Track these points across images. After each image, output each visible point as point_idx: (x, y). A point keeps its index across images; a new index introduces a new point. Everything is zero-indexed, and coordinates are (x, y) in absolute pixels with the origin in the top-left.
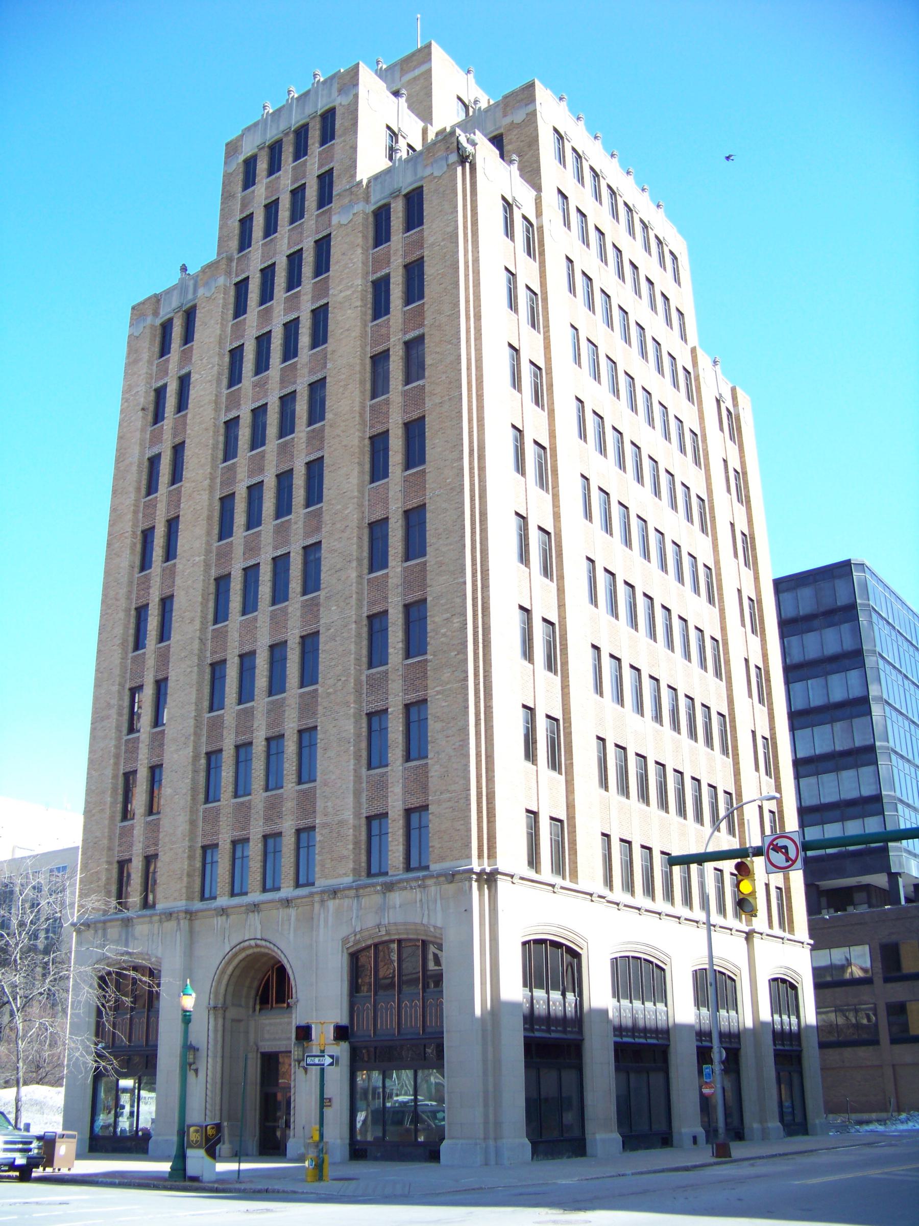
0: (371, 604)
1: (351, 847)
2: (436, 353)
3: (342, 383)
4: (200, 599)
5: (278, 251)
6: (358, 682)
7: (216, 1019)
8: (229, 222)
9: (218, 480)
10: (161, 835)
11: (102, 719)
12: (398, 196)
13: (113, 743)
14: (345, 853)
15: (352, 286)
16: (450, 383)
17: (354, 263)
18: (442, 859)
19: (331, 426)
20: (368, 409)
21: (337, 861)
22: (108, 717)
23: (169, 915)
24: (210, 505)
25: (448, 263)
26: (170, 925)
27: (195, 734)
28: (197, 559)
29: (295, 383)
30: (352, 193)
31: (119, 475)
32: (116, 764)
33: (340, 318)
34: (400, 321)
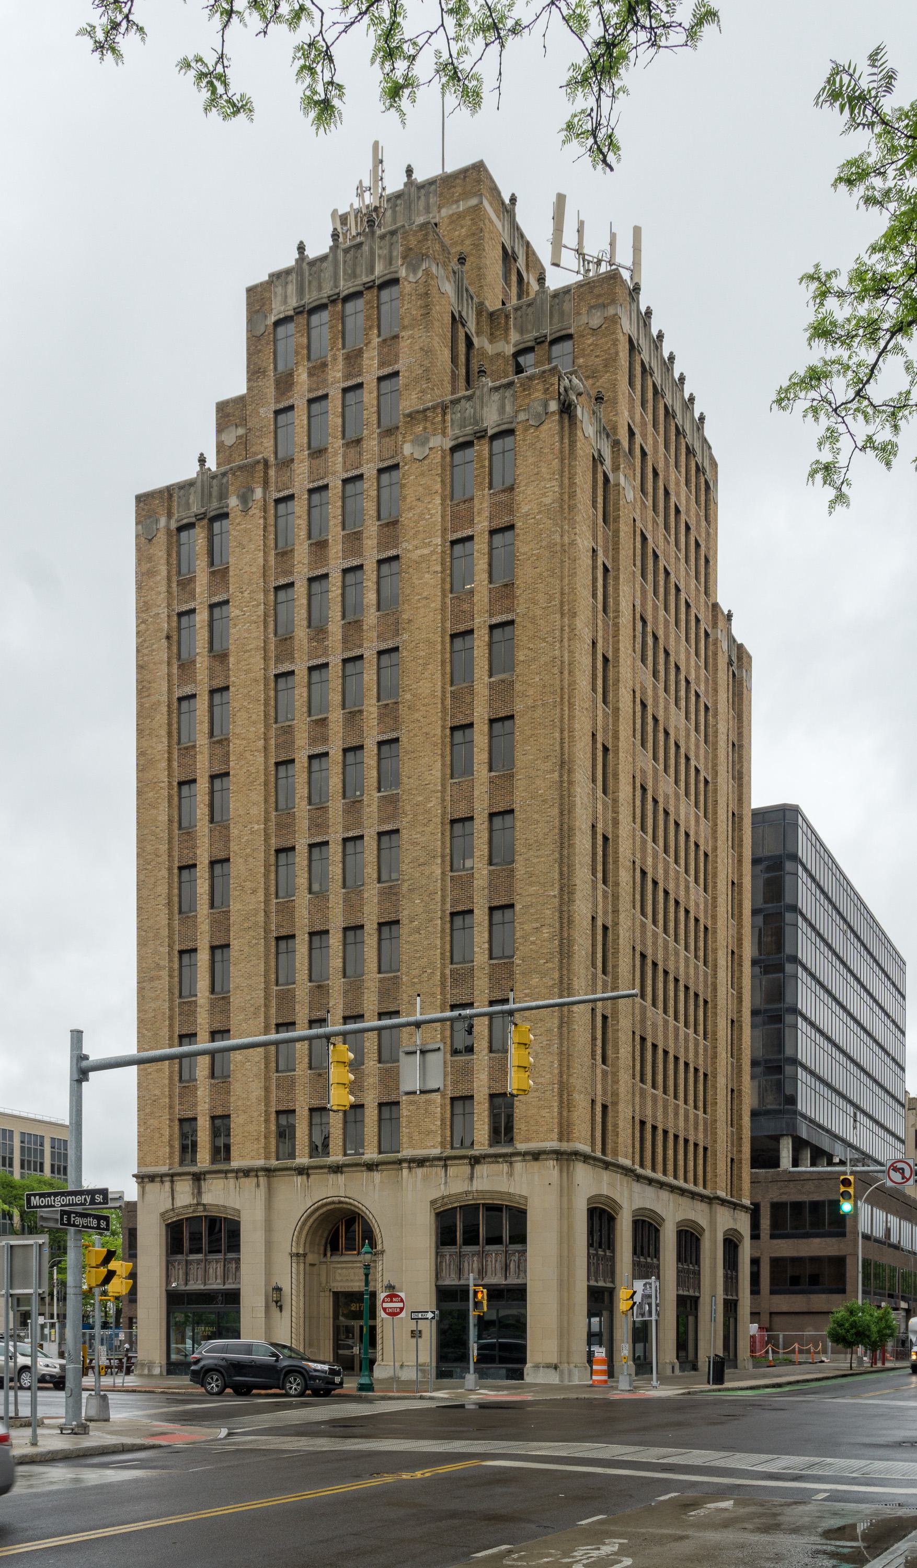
0: (455, 902)
1: (439, 1123)
2: (529, 649)
3: (420, 661)
4: (262, 870)
5: (331, 470)
6: (443, 975)
7: (298, 1263)
8: (262, 411)
9: (273, 742)
10: (232, 1099)
11: (152, 979)
12: (483, 437)
13: (167, 1005)
14: (433, 1128)
15: (429, 544)
16: (544, 686)
17: (432, 515)
18: (528, 1140)
19: (409, 708)
20: (448, 695)
21: (423, 1133)
22: (159, 978)
23: (246, 1173)
24: (266, 769)
25: (544, 543)
26: (249, 1182)
27: (266, 1005)
28: (256, 827)
29: (361, 646)
30: (426, 419)
31: (143, 714)
32: (171, 1026)
33: (417, 582)
34: (486, 600)
